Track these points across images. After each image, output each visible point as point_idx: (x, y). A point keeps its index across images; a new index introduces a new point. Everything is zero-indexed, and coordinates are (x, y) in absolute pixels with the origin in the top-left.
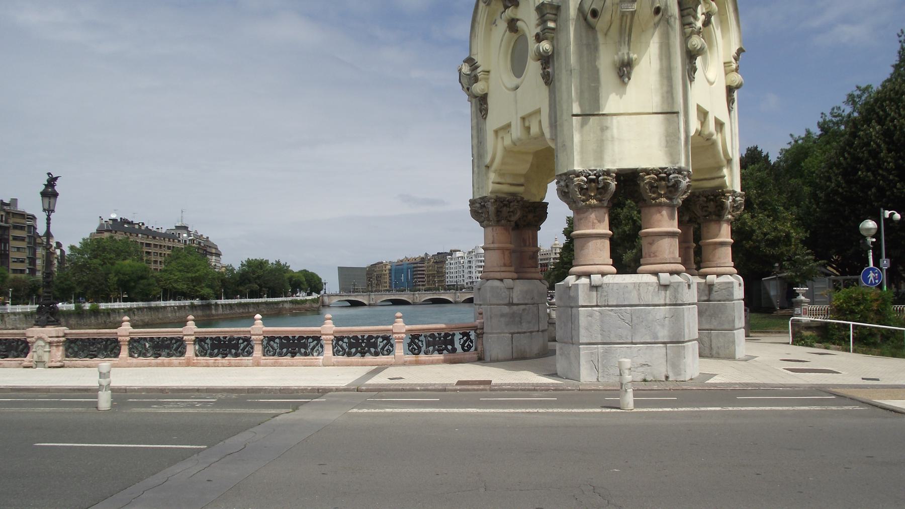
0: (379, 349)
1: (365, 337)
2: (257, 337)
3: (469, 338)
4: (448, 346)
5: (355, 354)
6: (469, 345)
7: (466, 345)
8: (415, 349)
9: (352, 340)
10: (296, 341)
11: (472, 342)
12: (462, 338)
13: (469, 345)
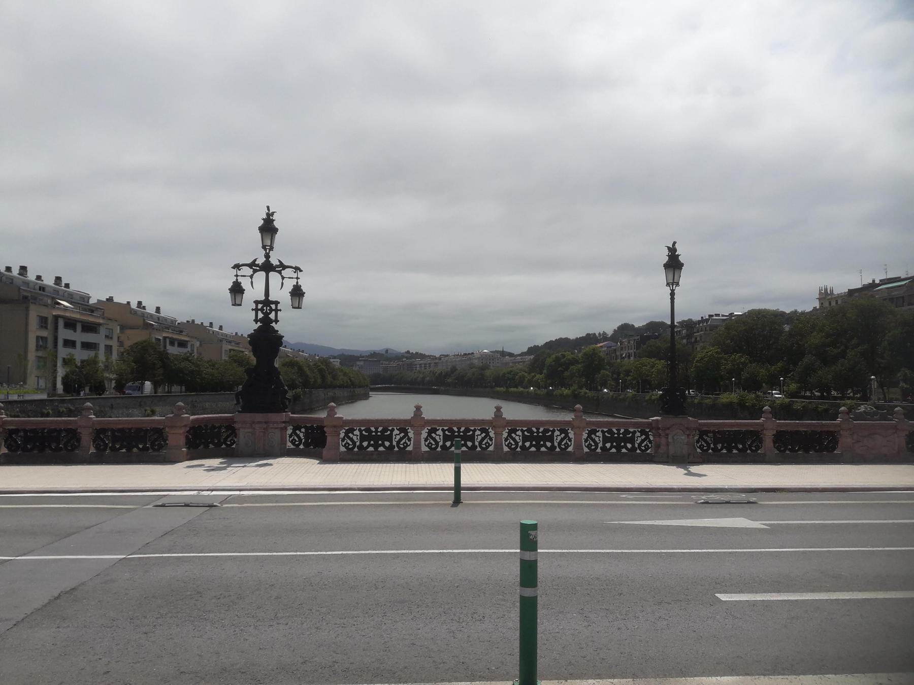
0: (636, 445)
3: (647, 437)
4: (610, 444)
5: (32, 449)
6: (566, 443)
7: (563, 443)
8: (296, 441)
9: (606, 434)
12: (480, 435)
13: (566, 443)
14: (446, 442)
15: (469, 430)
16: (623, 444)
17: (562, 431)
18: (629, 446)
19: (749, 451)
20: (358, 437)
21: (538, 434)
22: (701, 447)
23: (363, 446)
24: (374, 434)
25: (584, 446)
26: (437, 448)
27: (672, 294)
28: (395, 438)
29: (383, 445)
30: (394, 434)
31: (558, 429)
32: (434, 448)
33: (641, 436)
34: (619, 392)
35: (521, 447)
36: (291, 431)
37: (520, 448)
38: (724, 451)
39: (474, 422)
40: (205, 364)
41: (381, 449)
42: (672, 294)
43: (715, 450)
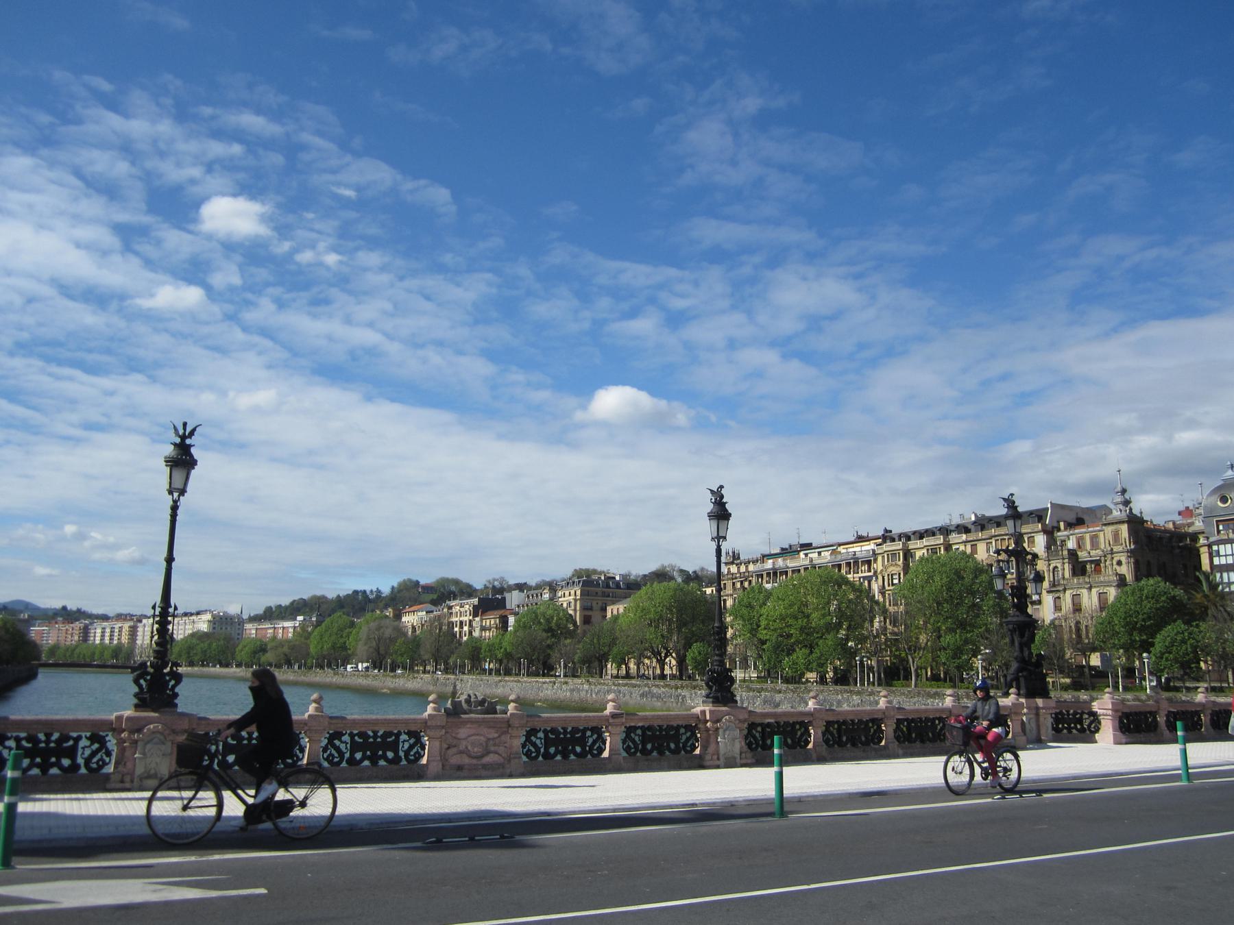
1: (379, 734)
2: (1105, 711)
6: (101, 759)
8: (532, 752)
9: (356, 738)
10: (1071, 717)
11: (109, 754)
12: (89, 746)
13: (101, 759)
14: (355, 753)
15: (68, 738)
16: (380, 753)
17: (94, 738)
18: (390, 755)
19: (589, 756)
20: (348, 746)
21: (375, 739)
22: (528, 754)
23: (356, 758)
24: (371, 740)
25: (322, 760)
26: (342, 762)
27: (175, 508)
28: (403, 747)
29: (58, 764)
30: (401, 740)
31: (406, 731)
32: (535, 756)
33: (92, 744)
34: (1053, 682)
35: (347, 762)
36: (326, 741)
37: (542, 757)
38: (366, 763)
39: (78, 724)
40: (536, 654)
41: (54, 771)
42: (175, 508)
43: (352, 761)
